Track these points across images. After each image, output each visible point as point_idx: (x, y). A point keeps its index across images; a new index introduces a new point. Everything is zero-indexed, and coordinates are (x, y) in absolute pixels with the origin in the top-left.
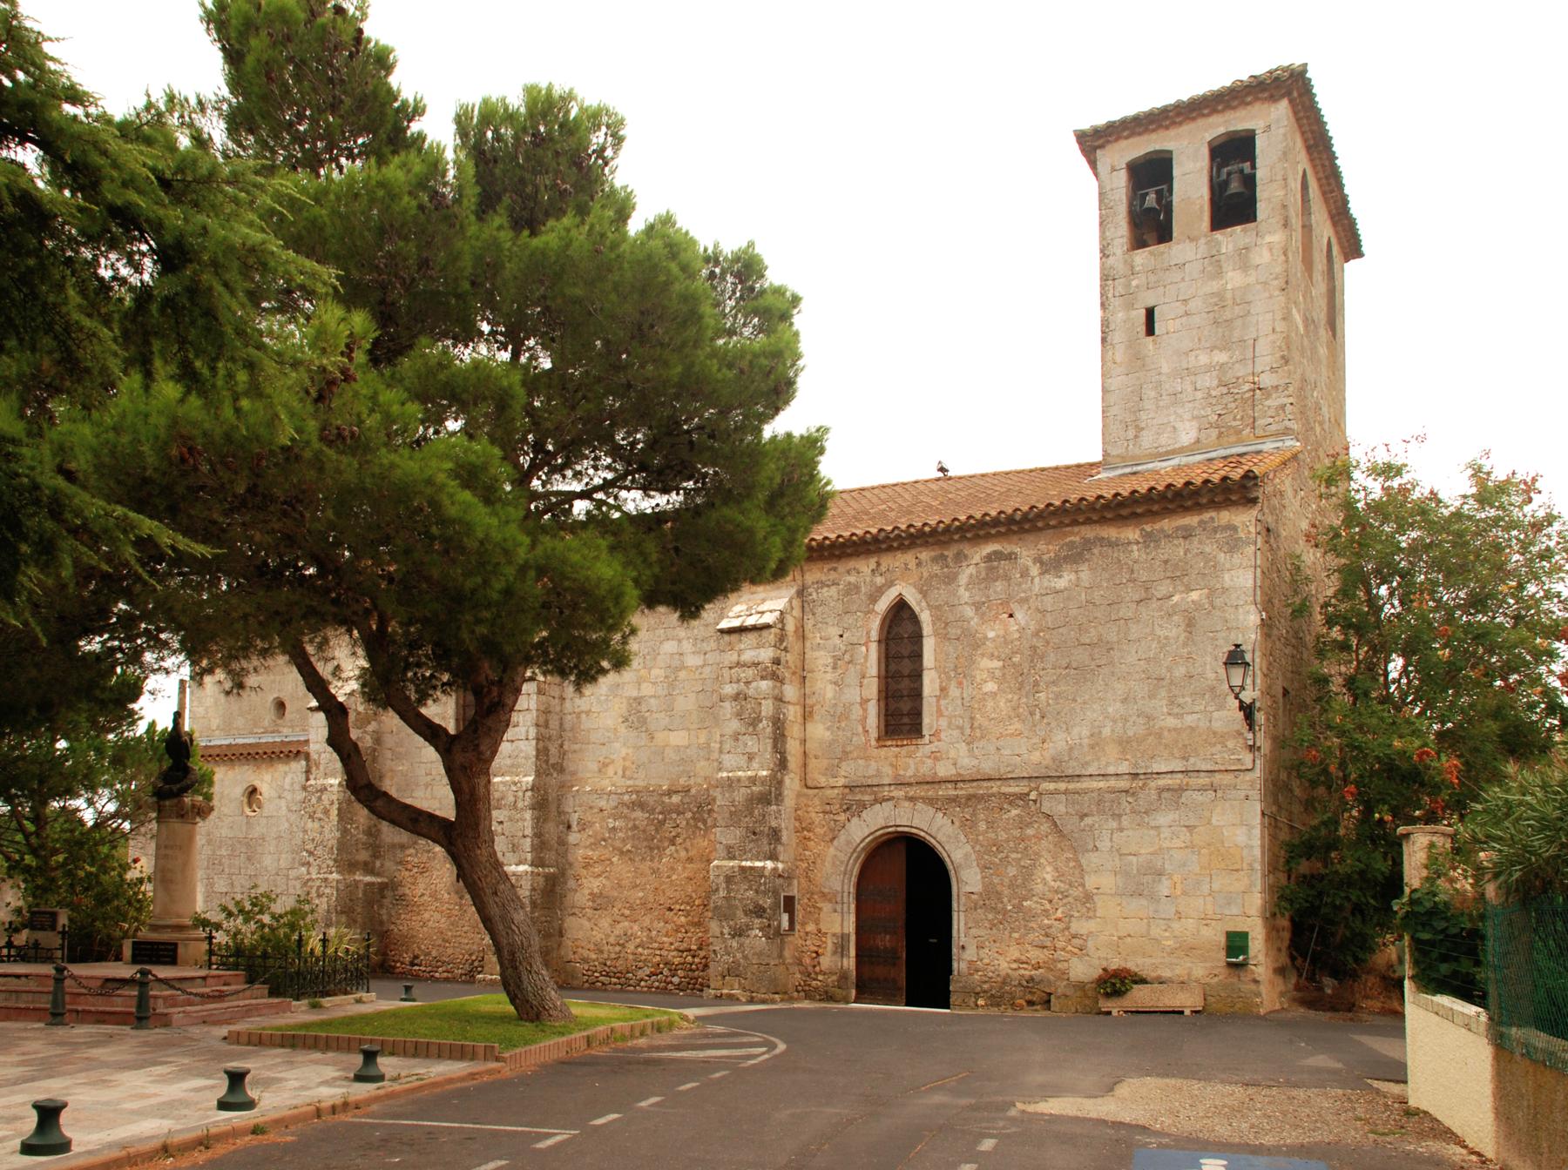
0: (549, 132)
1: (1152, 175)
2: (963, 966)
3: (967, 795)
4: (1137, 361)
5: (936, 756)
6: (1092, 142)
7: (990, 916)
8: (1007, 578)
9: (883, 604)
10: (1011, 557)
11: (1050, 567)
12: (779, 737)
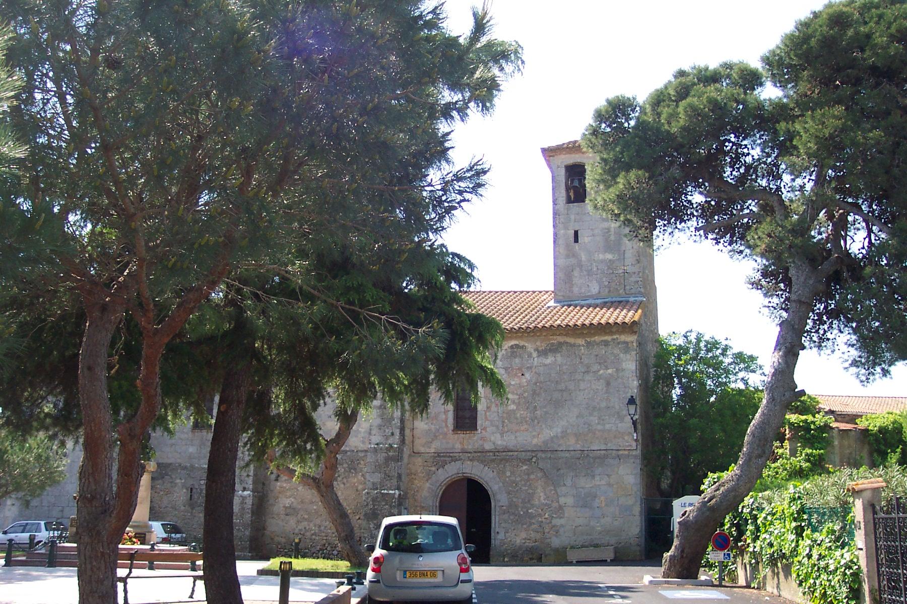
0: (212, 71)
1: (576, 172)
2: (497, 543)
3: (499, 457)
4: (571, 254)
5: (482, 438)
6: (549, 153)
7: (512, 517)
8: (521, 357)
10: (523, 347)
11: (543, 353)
12: (402, 429)
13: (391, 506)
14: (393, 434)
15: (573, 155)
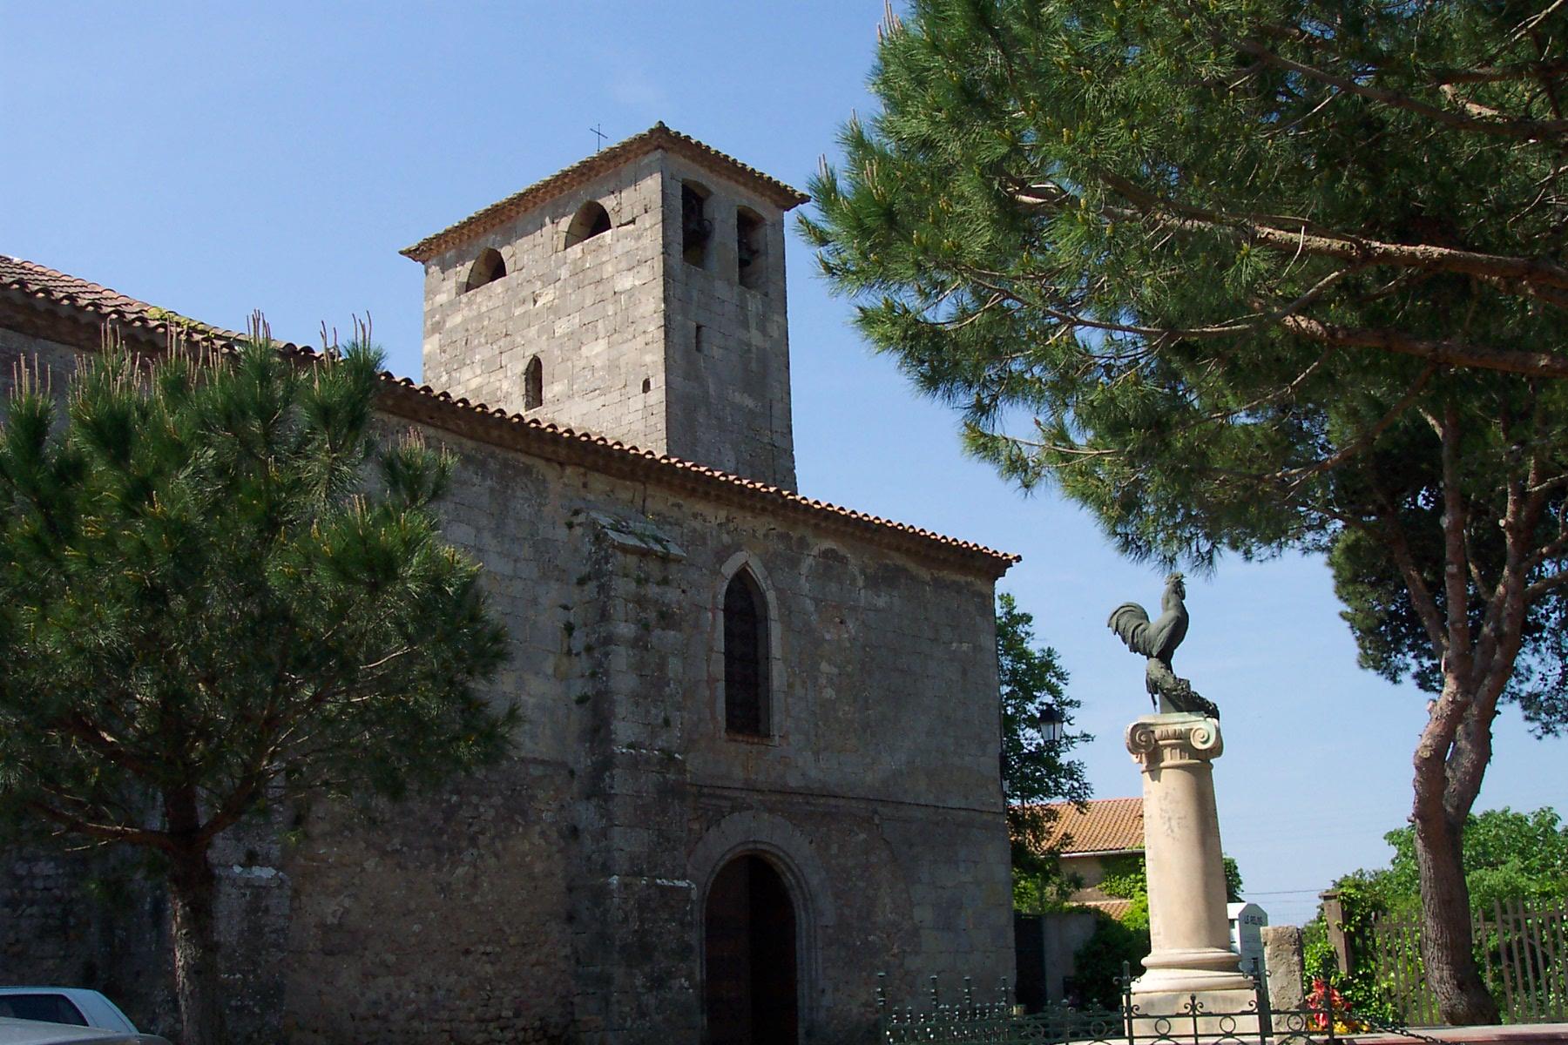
3: (813, 806)
9: (730, 568)
11: (873, 582)
13: (682, 924)
14: (667, 722)
15: (697, 167)
